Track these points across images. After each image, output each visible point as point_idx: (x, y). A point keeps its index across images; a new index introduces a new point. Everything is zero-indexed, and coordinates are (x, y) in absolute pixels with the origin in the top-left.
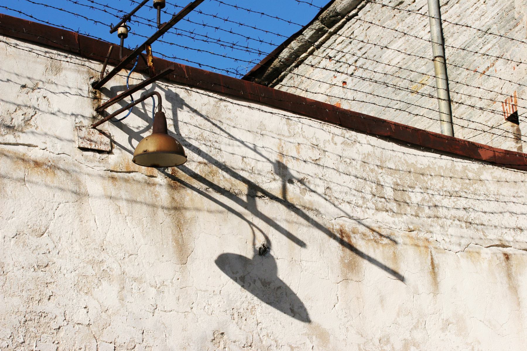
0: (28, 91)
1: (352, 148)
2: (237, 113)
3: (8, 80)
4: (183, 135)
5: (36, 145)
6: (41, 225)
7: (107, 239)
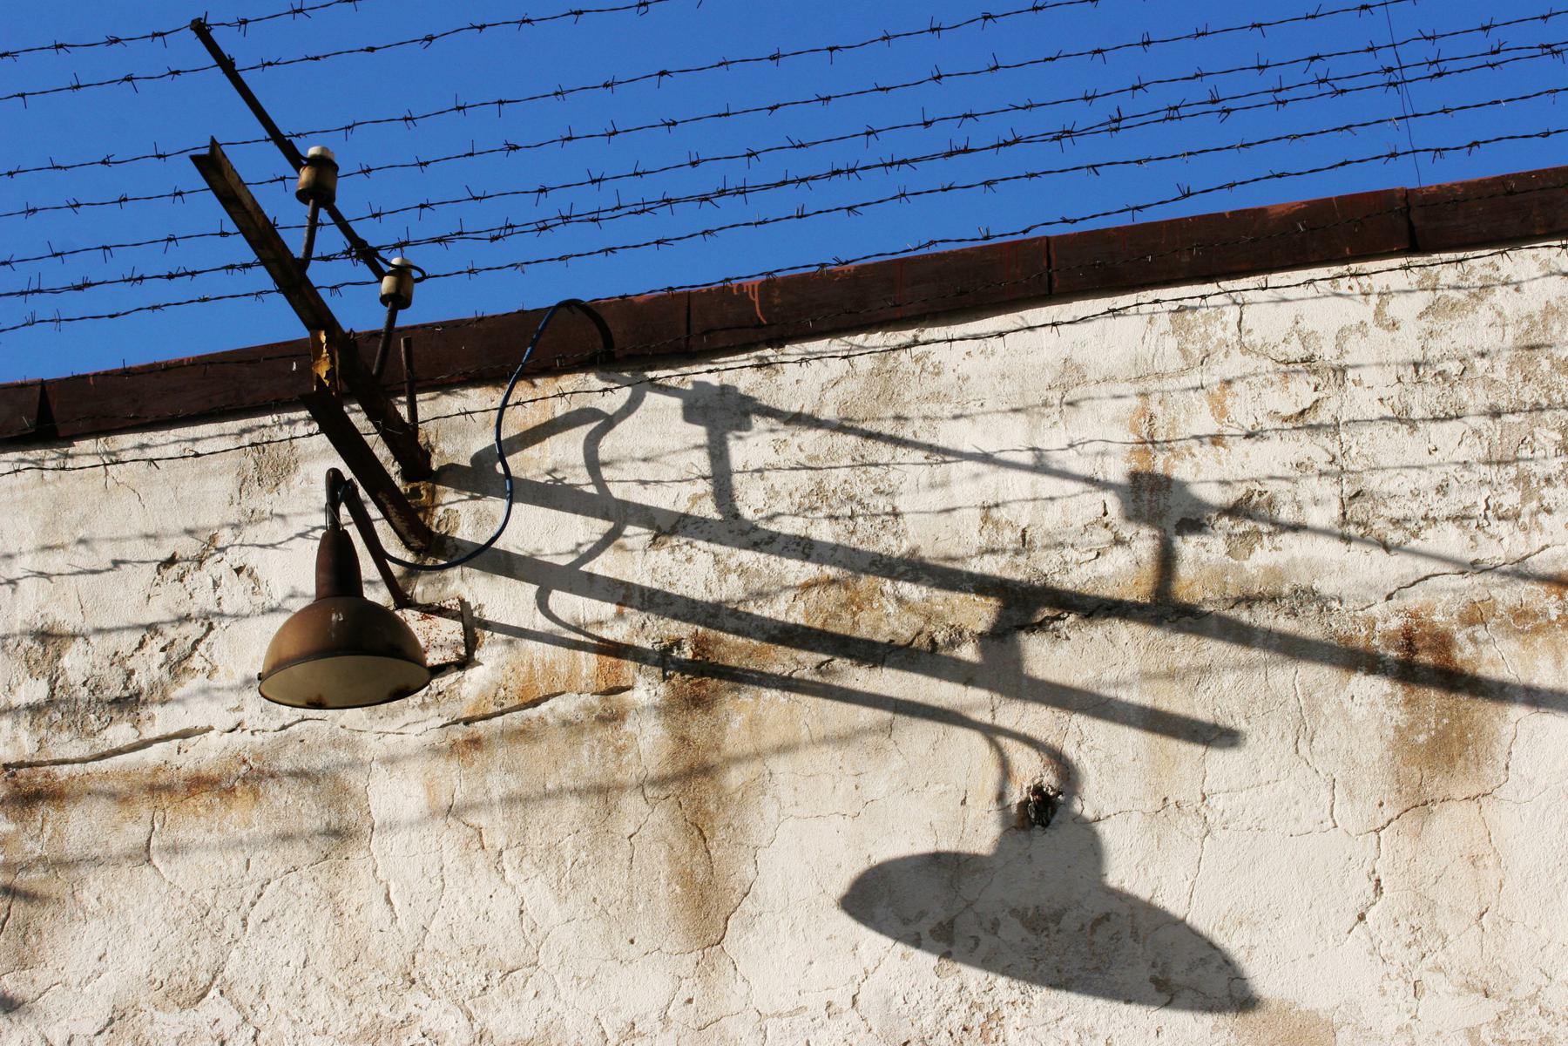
0: (181, 572)
1: (1471, 316)
2: (966, 367)
3: (116, 563)
4: (747, 514)
5: (205, 725)
6: (197, 969)
7: (428, 946)
